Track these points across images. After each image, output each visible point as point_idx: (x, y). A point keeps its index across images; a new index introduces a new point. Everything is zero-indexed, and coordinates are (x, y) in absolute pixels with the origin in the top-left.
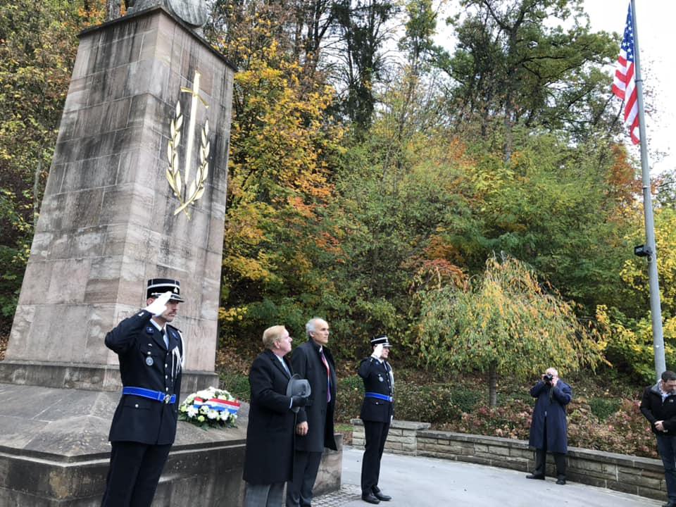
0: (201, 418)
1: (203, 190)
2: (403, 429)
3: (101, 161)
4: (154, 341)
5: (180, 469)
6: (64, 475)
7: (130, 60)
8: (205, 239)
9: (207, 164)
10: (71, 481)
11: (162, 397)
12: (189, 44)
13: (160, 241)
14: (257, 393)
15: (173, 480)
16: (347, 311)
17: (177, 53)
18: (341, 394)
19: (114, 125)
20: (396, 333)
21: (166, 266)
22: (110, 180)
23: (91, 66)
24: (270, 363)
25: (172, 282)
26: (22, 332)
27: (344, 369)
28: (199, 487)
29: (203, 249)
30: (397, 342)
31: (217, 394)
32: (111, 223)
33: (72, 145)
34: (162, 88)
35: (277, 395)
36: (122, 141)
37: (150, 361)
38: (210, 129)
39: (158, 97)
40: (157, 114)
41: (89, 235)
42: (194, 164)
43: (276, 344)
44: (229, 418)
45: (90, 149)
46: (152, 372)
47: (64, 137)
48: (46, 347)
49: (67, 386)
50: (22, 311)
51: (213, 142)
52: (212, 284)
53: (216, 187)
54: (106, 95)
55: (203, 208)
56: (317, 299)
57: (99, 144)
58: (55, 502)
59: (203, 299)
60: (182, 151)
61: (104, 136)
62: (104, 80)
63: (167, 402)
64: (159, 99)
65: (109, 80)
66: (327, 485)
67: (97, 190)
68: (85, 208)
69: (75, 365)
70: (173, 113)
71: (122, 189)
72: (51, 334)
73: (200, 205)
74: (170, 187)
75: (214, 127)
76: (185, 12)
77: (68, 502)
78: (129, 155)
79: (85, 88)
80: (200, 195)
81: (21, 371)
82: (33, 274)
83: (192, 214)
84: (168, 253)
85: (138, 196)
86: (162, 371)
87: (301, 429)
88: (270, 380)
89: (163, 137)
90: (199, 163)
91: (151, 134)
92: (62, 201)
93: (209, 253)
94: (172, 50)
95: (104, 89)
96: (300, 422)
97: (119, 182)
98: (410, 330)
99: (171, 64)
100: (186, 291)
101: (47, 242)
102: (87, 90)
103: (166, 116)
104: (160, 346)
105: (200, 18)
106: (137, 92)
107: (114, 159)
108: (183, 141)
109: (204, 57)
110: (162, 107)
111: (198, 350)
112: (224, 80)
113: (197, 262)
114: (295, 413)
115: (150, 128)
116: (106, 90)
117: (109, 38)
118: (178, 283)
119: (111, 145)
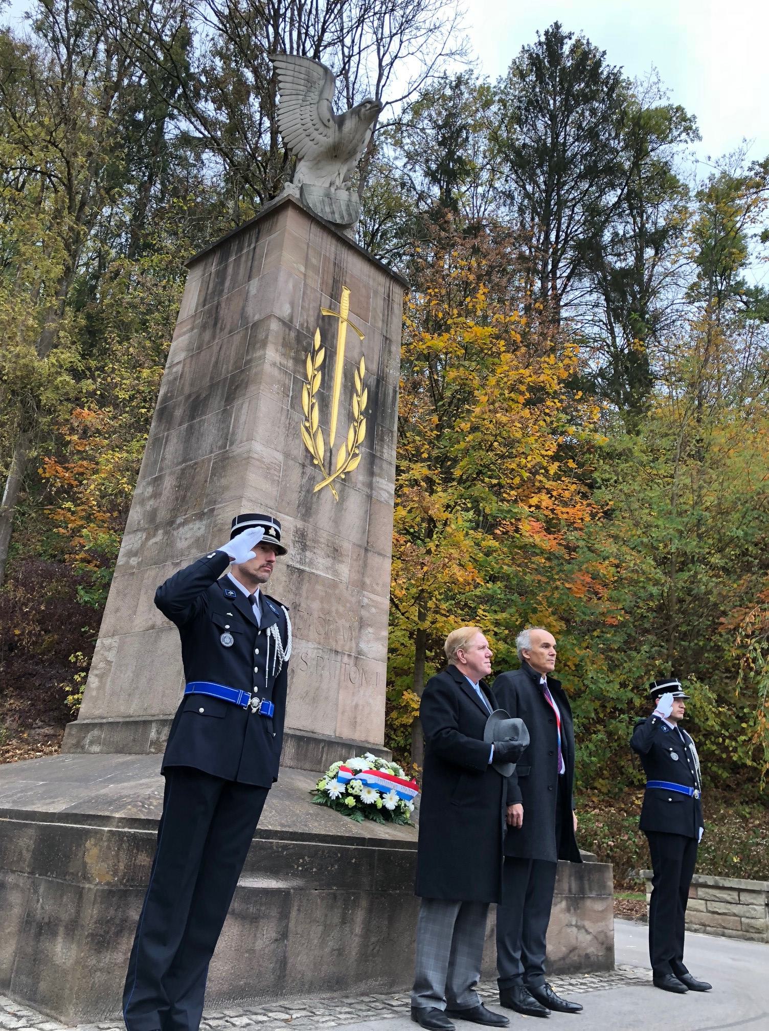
0: (350, 801)
1: (359, 458)
2: (740, 890)
3: (210, 421)
4: (236, 609)
5: (305, 871)
6: (106, 844)
7: (250, 278)
8: (364, 532)
9: (364, 421)
10: (117, 855)
11: (245, 699)
12: (333, 249)
13: (293, 529)
14: (431, 734)
15: (294, 889)
16: (630, 702)
17: (314, 261)
18: (626, 838)
19: (226, 369)
20: (721, 740)
21: (302, 567)
22: (220, 443)
23: (202, 299)
24: (455, 688)
25: (268, 519)
26: (101, 677)
27: (633, 803)
28: (340, 911)
29: (360, 546)
30: (724, 756)
31: (378, 766)
32: (220, 503)
33: (174, 408)
34: (293, 307)
35: (464, 739)
36: (237, 387)
37: (227, 640)
38: (366, 369)
39: (286, 320)
40: (285, 344)
41: (191, 526)
42: (344, 419)
43: (460, 655)
44: (398, 807)
45: (196, 406)
46: (230, 658)
47: (166, 399)
48: (129, 695)
49: (153, 750)
50: (103, 646)
51: (373, 389)
52: (377, 602)
53: (378, 454)
54: (218, 331)
55: (359, 485)
56: (576, 683)
57: (207, 398)
58: (89, 889)
59: (362, 624)
60: (324, 400)
61: (213, 387)
62: (217, 312)
63: (254, 710)
64: (287, 324)
65: (222, 312)
66: (587, 956)
67: (203, 461)
68: (187, 489)
69: (165, 718)
70: (309, 344)
71: (235, 453)
72: (137, 675)
73: (353, 480)
74: (307, 450)
75: (374, 367)
76: (328, 209)
77: (110, 891)
78: (245, 406)
79: (192, 329)
80: (353, 465)
81: (96, 732)
82: (118, 592)
83: (342, 493)
84: (304, 548)
85: (258, 460)
86: (248, 658)
87: (512, 815)
88: (452, 713)
89: (294, 377)
90: (351, 417)
91: (276, 372)
92: (158, 485)
93: (370, 554)
94: (307, 254)
95: (215, 324)
96: (511, 802)
97: (232, 444)
98: (746, 735)
99: (305, 275)
100: (334, 609)
101: (137, 545)
102: (196, 331)
103: (300, 347)
104: (249, 622)
105: (350, 215)
106: (257, 318)
107: (226, 414)
108: (327, 384)
109: (356, 266)
110: (293, 334)
111: (356, 706)
112: (388, 299)
113: (352, 567)
114: (502, 777)
115: (274, 364)
116: (219, 325)
117: (224, 259)
118: (276, 522)
119: (222, 395)
